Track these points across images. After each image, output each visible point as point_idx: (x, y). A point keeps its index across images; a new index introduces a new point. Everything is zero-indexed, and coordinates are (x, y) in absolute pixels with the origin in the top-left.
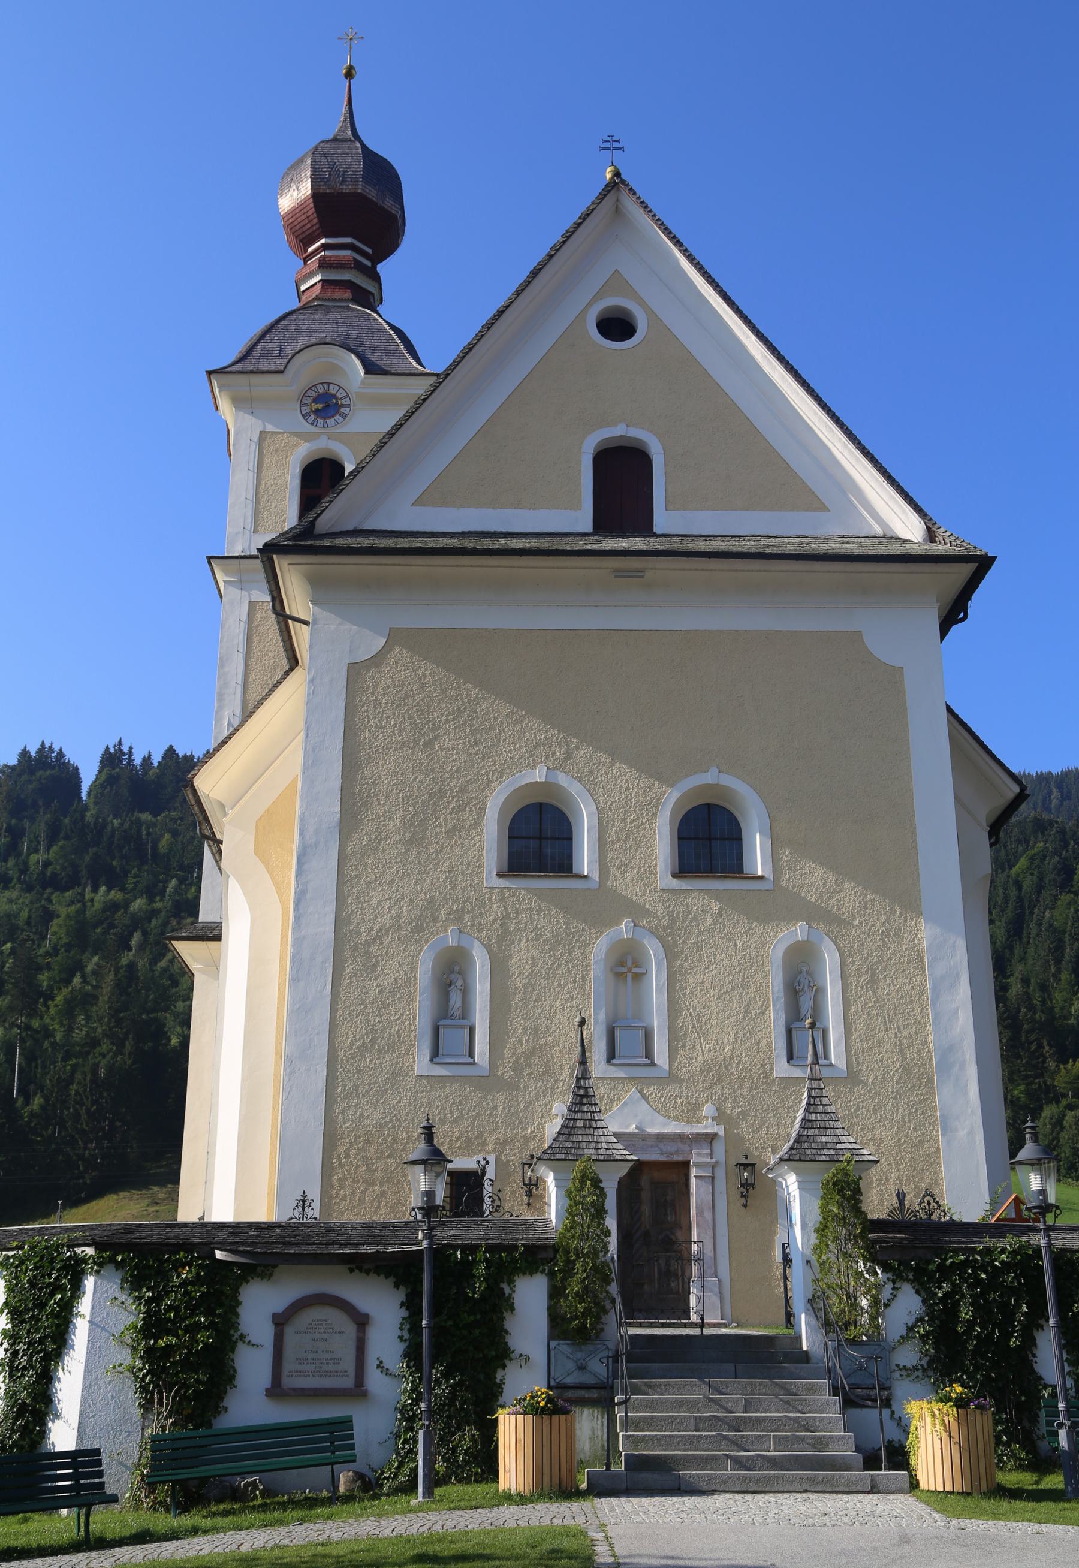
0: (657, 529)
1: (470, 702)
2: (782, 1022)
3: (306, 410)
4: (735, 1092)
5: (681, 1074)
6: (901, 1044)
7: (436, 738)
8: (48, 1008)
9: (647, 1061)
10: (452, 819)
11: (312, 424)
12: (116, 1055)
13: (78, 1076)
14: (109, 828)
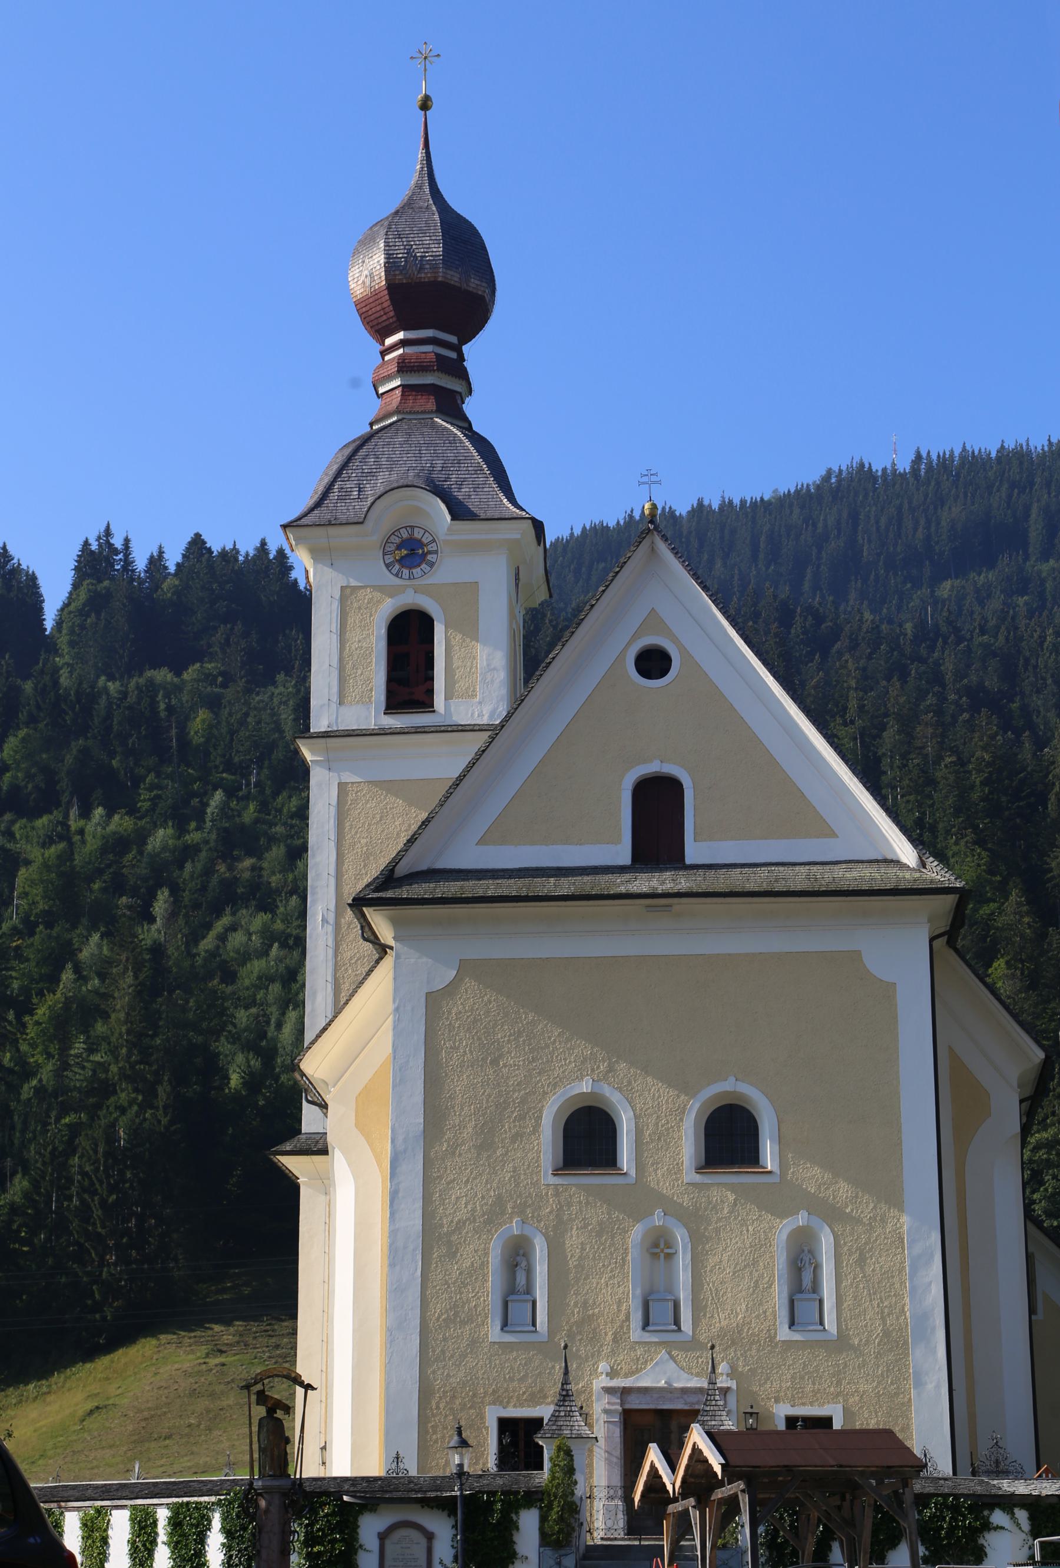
0: (688, 861)
1: (528, 1023)
2: (785, 1295)
3: (389, 559)
4: (745, 1352)
5: (702, 1338)
6: (882, 1312)
7: (501, 1056)
8: (24, 1026)
9: (674, 1327)
10: (515, 1126)
11: (397, 575)
12: (142, 1108)
13: (83, 1142)
14: (103, 701)
